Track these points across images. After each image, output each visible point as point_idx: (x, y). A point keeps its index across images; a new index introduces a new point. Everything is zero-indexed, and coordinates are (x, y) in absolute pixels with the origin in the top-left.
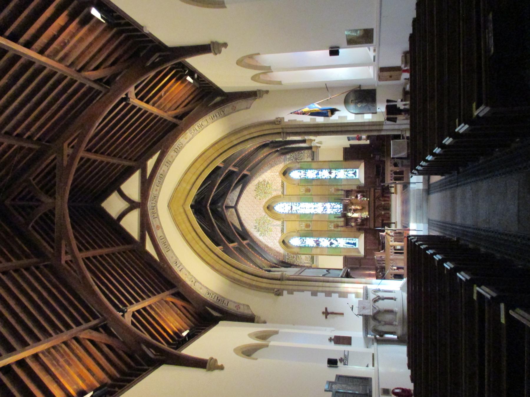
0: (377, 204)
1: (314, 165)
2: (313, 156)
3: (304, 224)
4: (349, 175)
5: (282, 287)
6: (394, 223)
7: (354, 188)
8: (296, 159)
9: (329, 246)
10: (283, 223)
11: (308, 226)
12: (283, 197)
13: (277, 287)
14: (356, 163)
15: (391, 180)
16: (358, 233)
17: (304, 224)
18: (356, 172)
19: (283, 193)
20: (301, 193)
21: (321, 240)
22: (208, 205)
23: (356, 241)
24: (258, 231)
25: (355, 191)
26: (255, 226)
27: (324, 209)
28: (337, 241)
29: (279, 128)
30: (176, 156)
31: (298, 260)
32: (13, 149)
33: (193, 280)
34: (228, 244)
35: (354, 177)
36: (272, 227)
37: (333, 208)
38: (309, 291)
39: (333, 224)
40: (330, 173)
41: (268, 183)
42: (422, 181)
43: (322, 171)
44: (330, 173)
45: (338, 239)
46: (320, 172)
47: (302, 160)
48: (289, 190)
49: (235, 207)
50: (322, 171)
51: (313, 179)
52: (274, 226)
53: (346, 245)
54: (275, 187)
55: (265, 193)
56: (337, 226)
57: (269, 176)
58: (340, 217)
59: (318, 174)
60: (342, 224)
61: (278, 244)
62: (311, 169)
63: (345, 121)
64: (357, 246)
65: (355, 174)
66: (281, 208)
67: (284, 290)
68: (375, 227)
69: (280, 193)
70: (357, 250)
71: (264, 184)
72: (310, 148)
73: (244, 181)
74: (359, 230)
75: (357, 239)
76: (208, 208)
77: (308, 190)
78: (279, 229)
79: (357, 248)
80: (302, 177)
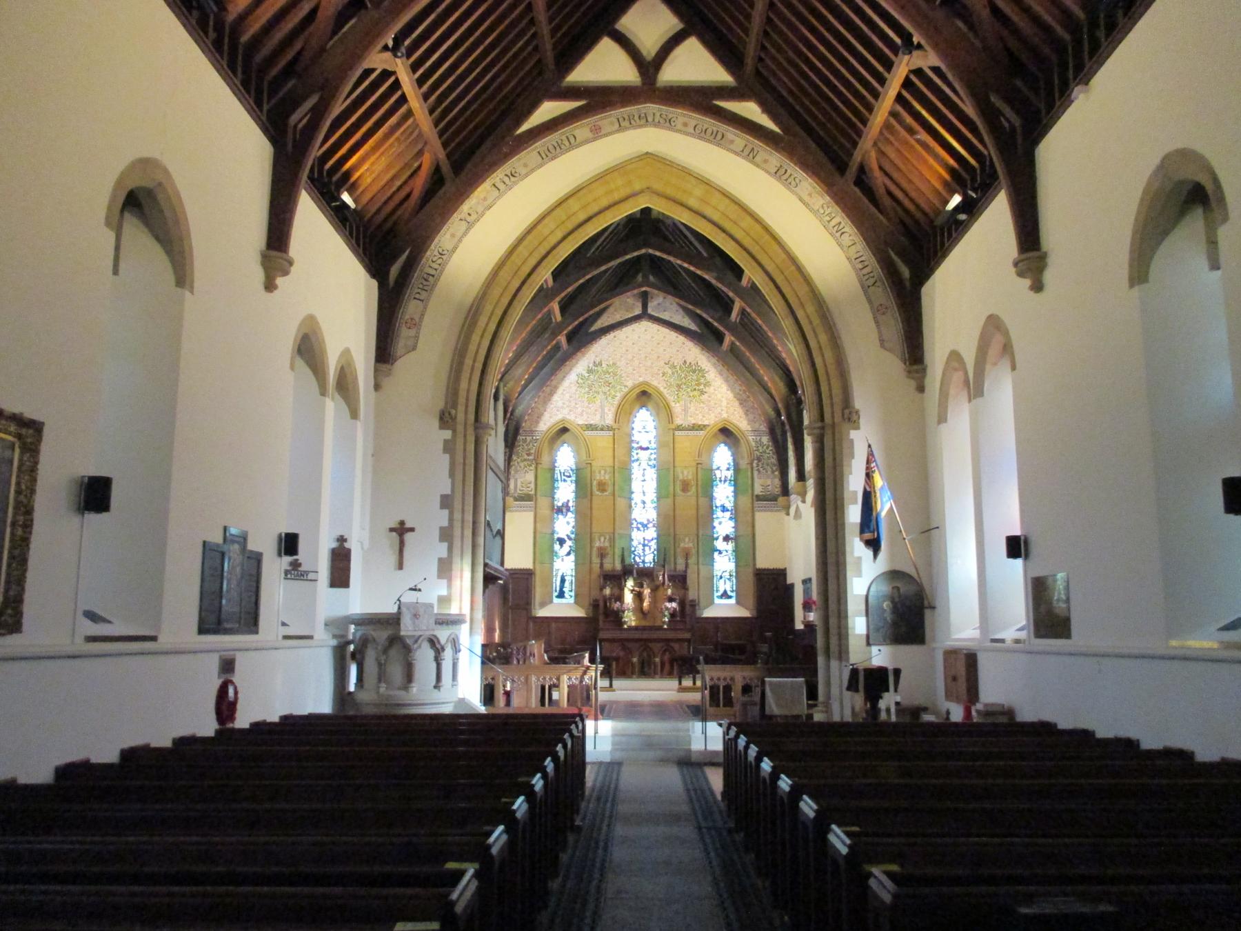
0: (630, 645)
1: (745, 501)
2: (767, 499)
5: (460, 428)
6: (611, 685)
7: (692, 595)
8: (759, 459)
9: (556, 536)
10: (609, 428)
11: (602, 486)
12: (669, 427)
13: (460, 416)
14: (751, 600)
15: (712, 679)
16: (587, 602)
17: (607, 477)
18: (730, 597)
19: (679, 428)
20: (678, 470)
21: (571, 517)
22: (651, 251)
23: (569, 598)
24: (590, 371)
25: (685, 595)
26: (600, 364)
27: (642, 524)
28: (569, 554)
29: (833, 417)
30: (767, 172)
31: (522, 465)
33: (474, 217)
34: (558, 299)
35: (716, 594)
36: (598, 402)
37: (644, 545)
38: (453, 491)
39: (607, 544)
40: (727, 538)
41: (702, 393)
42: (710, 748)
44: (727, 538)
45: (572, 557)
46: (728, 514)
47: (756, 473)
48: (686, 443)
49: (644, 315)
51: (711, 498)
52: (602, 407)
54: (692, 409)
55: (679, 386)
56: (602, 555)
57: (719, 396)
58: (623, 560)
59: (724, 509)
60: (608, 566)
61: (560, 417)
62: (736, 492)
63: (849, 574)
64: (556, 600)
65: (725, 595)
66: (644, 424)
67: (454, 431)
68: (601, 641)
69: (678, 421)
70: (547, 602)
71: (699, 385)
72: (785, 491)
73: (708, 337)
74: (595, 605)
75: (572, 601)
76: (643, 251)
77: (685, 487)
78: (595, 420)
79: (551, 602)
80: (718, 473)
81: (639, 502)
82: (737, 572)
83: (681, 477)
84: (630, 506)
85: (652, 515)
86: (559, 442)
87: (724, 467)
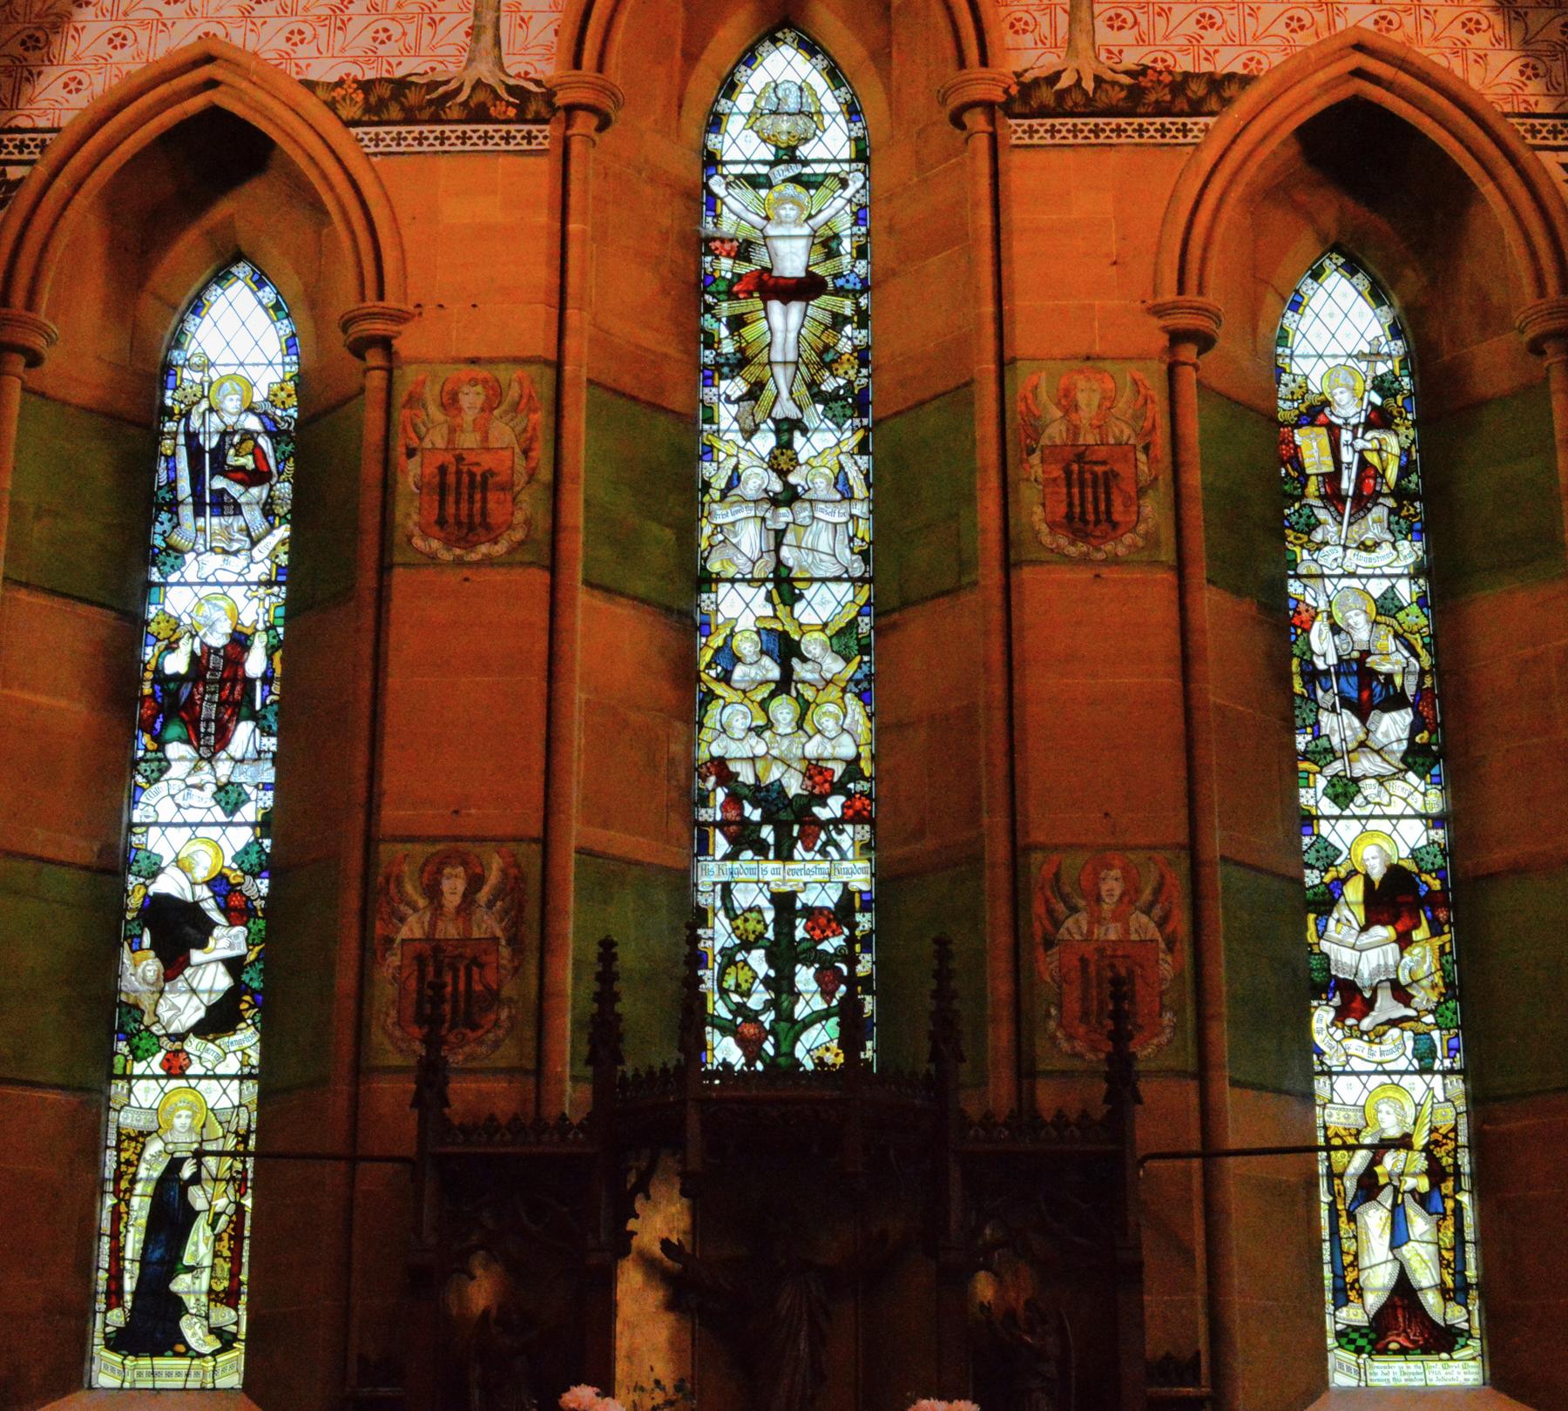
3: (499, 440)
4: (1375, 1219)
10: (530, 104)
11: (464, 498)
17: (503, 433)
18: (1441, 1340)
19: (1033, 98)
27: (769, 797)
28: (219, 1020)
32: (1329, 1296)
37: (784, 955)
39: (487, 924)
40: (1393, 899)
43: (1416, 758)
44: (1393, 899)
45: (246, 1040)
46: (1393, 726)
50: (1416, 758)
51: (1282, 623)
53: (150, 1170)
58: (604, 1033)
59: (1367, 691)
60: (480, 1088)
62: (1443, 579)
65: (1403, 1323)
75: (230, 1372)
78: (437, 53)
79: (71, 1372)
80: (1312, 448)
81: (746, 646)
82: (1478, 1144)
83: (1055, 432)
84: (685, 673)
85: (842, 733)
86: (188, 245)
87: (1348, 408)
